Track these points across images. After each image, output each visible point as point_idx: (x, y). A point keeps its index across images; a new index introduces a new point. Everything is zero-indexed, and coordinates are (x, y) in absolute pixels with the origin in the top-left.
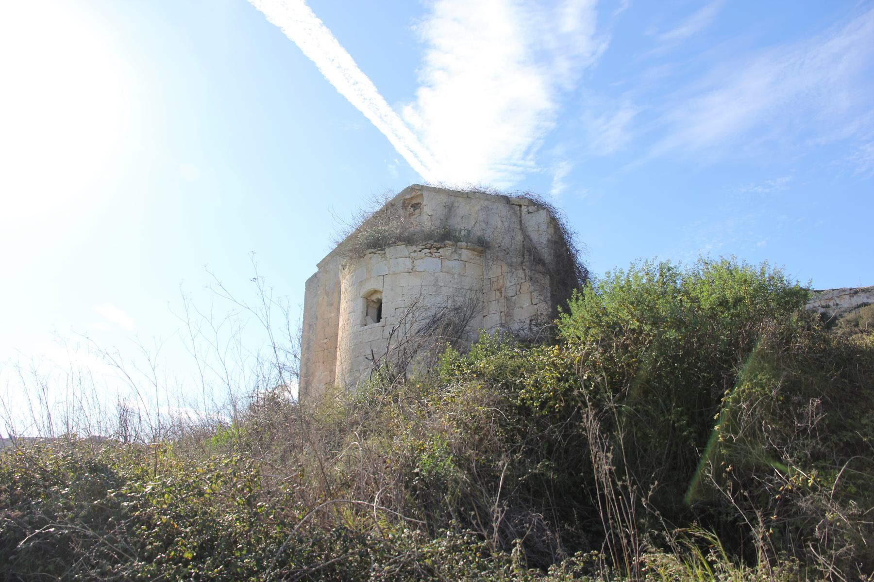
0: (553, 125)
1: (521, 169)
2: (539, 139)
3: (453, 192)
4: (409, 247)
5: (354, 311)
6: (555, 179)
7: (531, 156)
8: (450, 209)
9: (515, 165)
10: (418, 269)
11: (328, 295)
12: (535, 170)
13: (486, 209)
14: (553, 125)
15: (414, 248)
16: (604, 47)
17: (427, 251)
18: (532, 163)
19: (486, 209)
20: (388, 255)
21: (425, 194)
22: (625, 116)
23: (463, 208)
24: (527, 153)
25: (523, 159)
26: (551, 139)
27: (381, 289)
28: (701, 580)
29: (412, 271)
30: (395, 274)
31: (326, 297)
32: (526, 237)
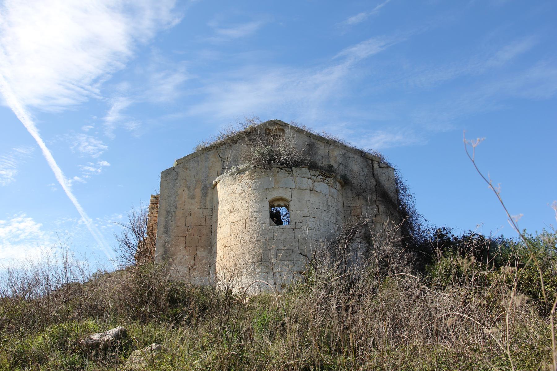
0: (123, 66)
1: (85, 92)
2: (108, 73)
3: (315, 136)
4: (311, 171)
5: (260, 211)
6: (113, 108)
7: (98, 85)
8: (311, 146)
9: (82, 88)
10: (317, 189)
11: (189, 189)
12: (98, 97)
13: (344, 155)
14: (123, 66)
15: (314, 173)
16: (177, 21)
17: (321, 177)
18: (97, 91)
19: (344, 155)
20: (295, 173)
21: (286, 130)
22: (179, 78)
23: (322, 150)
24: (95, 81)
25: (91, 85)
26: (118, 77)
27: (290, 199)
28: (513, 370)
29: (312, 190)
30: (300, 189)
31: (186, 190)
32: (378, 183)
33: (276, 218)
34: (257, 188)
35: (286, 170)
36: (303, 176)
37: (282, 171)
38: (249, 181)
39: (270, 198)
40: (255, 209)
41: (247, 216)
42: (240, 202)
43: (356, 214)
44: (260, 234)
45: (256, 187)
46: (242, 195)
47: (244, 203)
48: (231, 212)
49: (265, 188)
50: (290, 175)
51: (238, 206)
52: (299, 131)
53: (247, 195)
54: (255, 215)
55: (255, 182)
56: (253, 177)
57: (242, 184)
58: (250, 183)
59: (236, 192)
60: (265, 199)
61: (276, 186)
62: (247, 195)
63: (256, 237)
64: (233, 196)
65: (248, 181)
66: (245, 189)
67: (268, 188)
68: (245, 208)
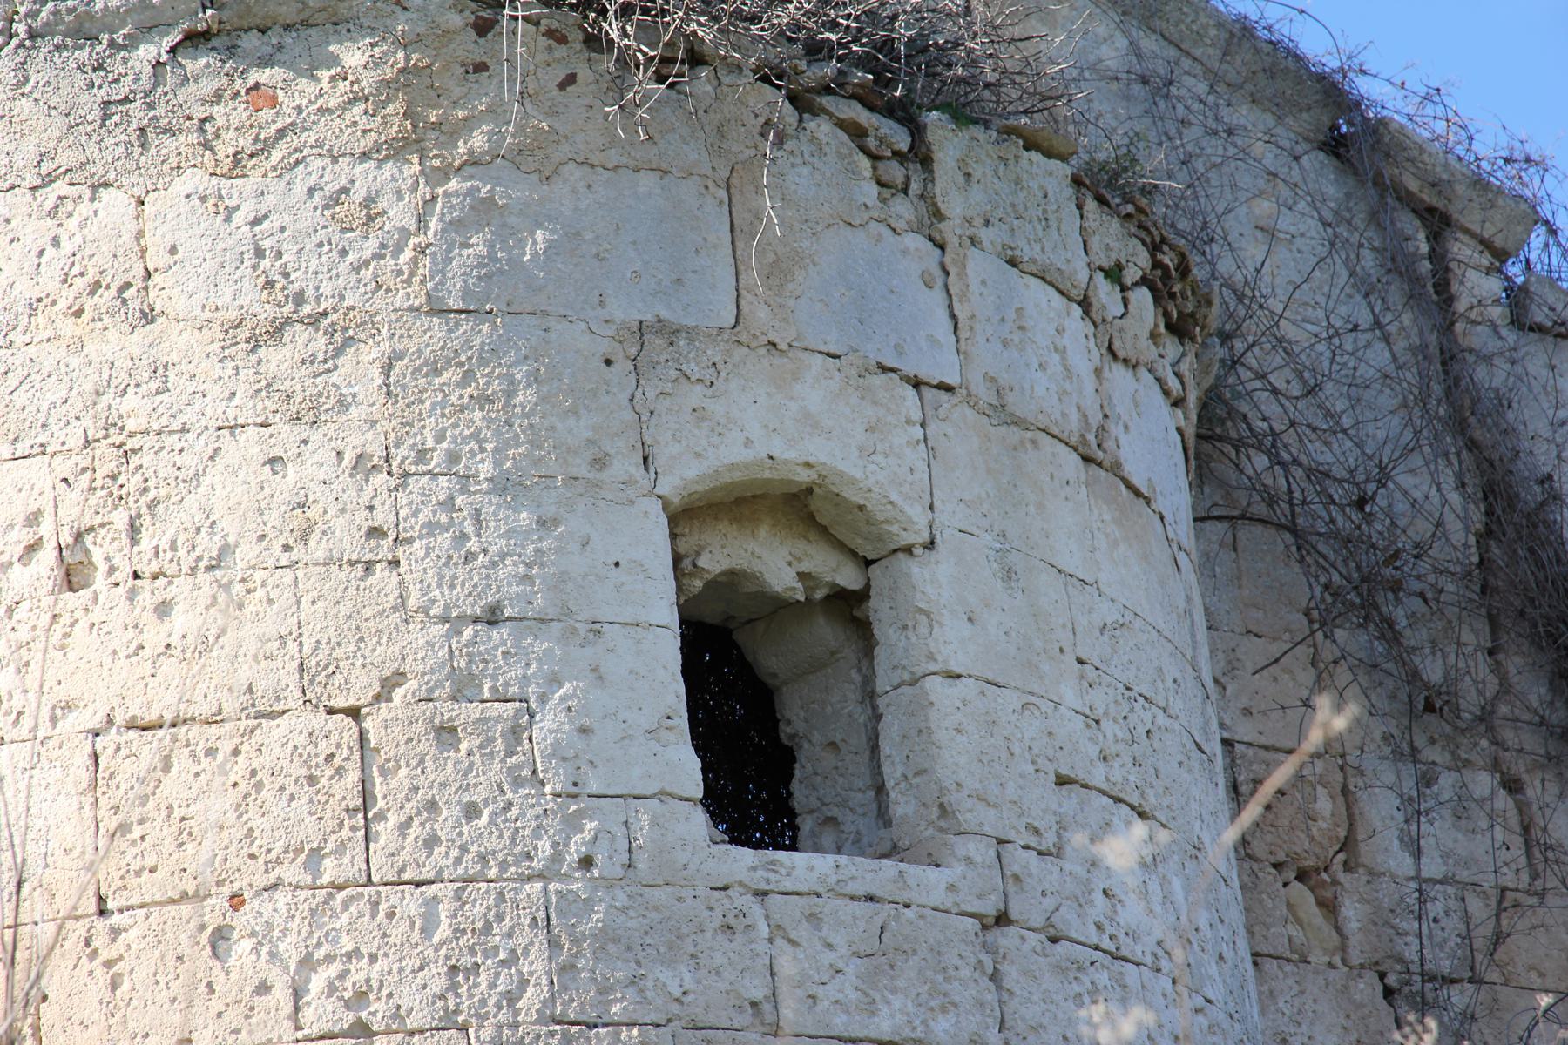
33: (753, 767)
34: (501, 299)
35: (857, 133)
36: (1026, 252)
37: (821, 128)
38: (396, 188)
39: (684, 472)
40: (505, 584)
41: (384, 655)
42: (250, 444)
43: (1301, 844)
44: (605, 938)
45: (490, 273)
46: (277, 359)
47: (315, 467)
48: (72, 577)
49: (627, 309)
50: (903, 209)
51: (228, 492)
52: (673, 536)
53: (360, 370)
54: (509, 659)
55: (482, 211)
56: (450, 132)
57: (285, 202)
58: (399, 214)
59: (169, 294)
60: (626, 465)
61: (759, 315)
62: (360, 370)
63: (536, 965)
64: (116, 344)
65: (365, 178)
66: (324, 279)
67: (670, 332)
68: (346, 537)
